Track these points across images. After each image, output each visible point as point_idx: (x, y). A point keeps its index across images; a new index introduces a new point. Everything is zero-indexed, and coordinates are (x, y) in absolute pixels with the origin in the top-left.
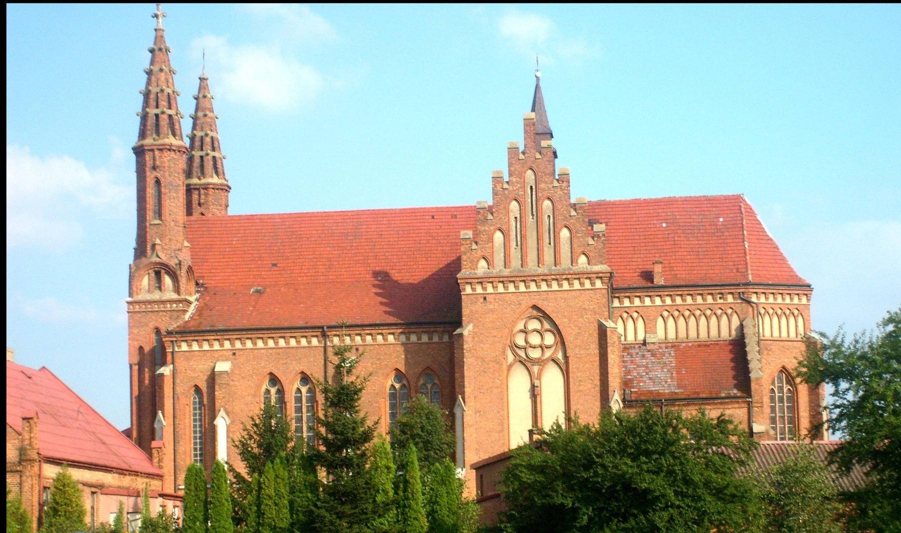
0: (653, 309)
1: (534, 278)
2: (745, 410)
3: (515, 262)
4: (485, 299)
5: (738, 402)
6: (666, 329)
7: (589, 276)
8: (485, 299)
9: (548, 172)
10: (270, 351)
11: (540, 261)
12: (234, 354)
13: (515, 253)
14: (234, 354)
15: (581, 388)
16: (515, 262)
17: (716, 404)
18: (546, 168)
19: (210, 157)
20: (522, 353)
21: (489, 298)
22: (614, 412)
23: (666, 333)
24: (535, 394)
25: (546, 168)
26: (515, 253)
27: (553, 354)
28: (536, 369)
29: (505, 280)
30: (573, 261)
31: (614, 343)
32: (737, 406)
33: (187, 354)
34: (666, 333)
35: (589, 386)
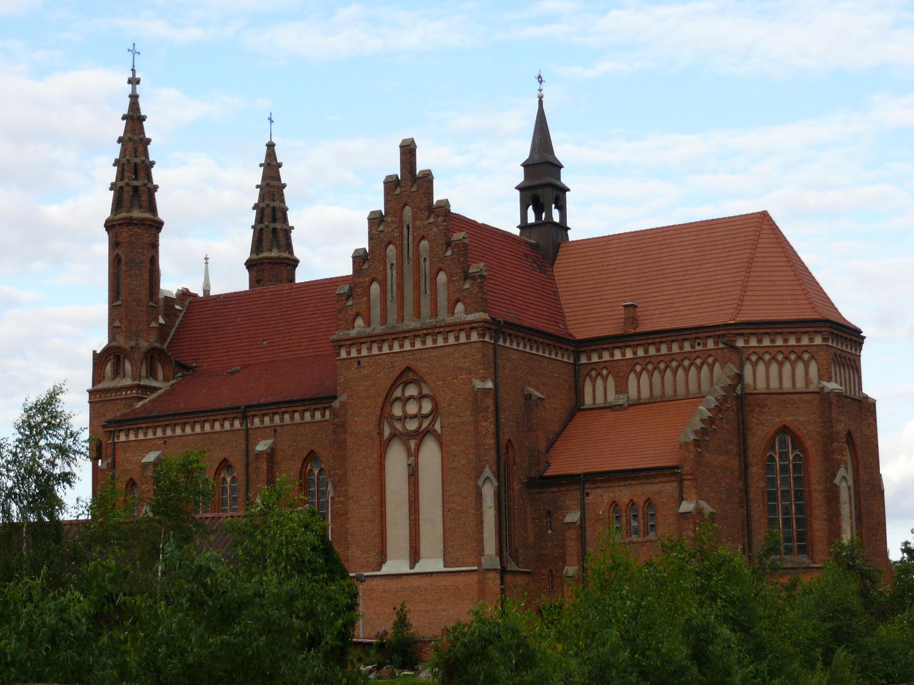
0: (624, 363)
1: (400, 336)
2: (675, 485)
3: (392, 318)
4: (359, 363)
5: (666, 475)
6: (639, 386)
7: (469, 327)
8: (359, 363)
9: (423, 206)
10: (196, 437)
11: (418, 315)
12: (165, 442)
13: (392, 307)
14: (165, 442)
15: (455, 464)
16: (392, 318)
17: (641, 478)
18: (421, 202)
19: (270, 230)
20: (399, 426)
21: (364, 362)
22: (151, 514)
23: (639, 392)
24: (413, 474)
25: (421, 202)
26: (392, 307)
27: (429, 425)
28: (413, 443)
29: (380, 339)
30: (451, 310)
31: (488, 407)
32: (665, 479)
33: (124, 445)
34: (639, 392)
35: (464, 462)
